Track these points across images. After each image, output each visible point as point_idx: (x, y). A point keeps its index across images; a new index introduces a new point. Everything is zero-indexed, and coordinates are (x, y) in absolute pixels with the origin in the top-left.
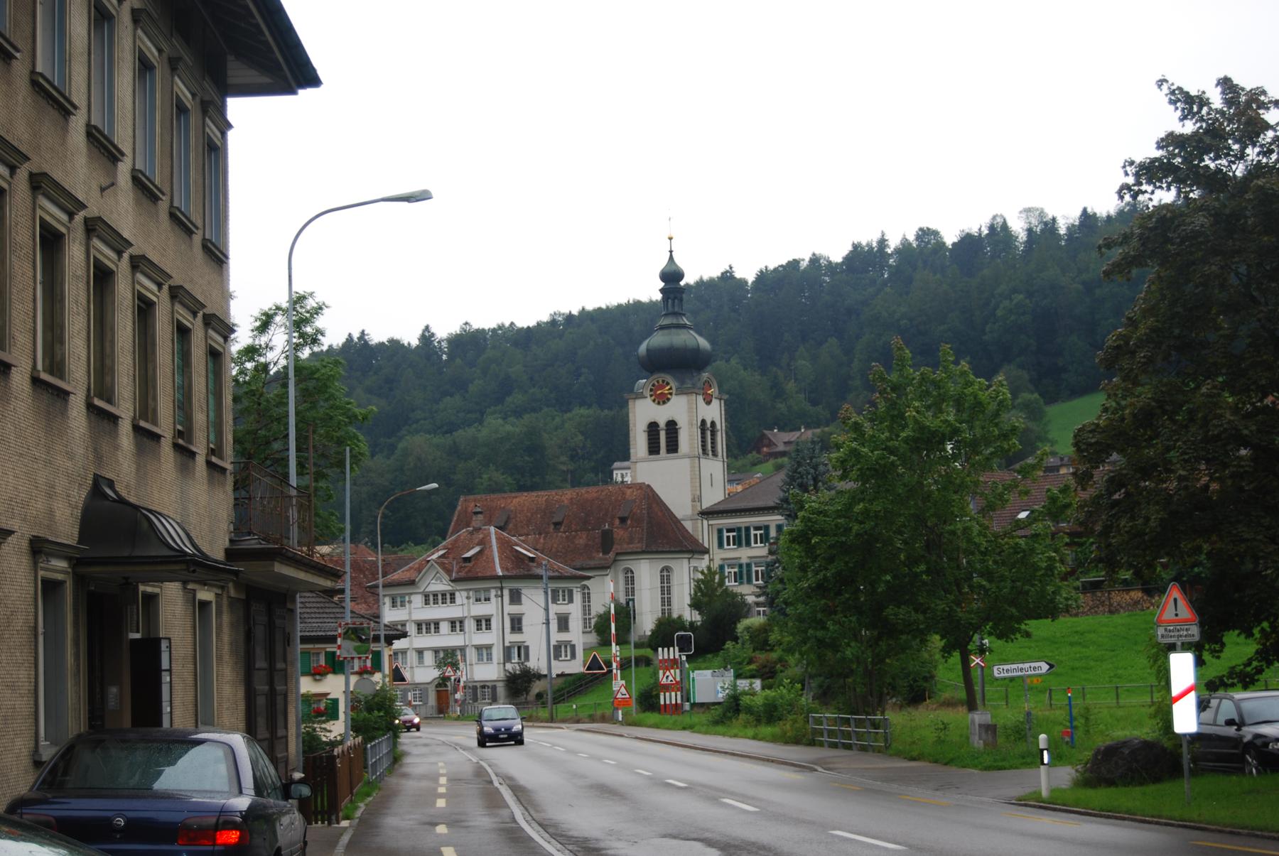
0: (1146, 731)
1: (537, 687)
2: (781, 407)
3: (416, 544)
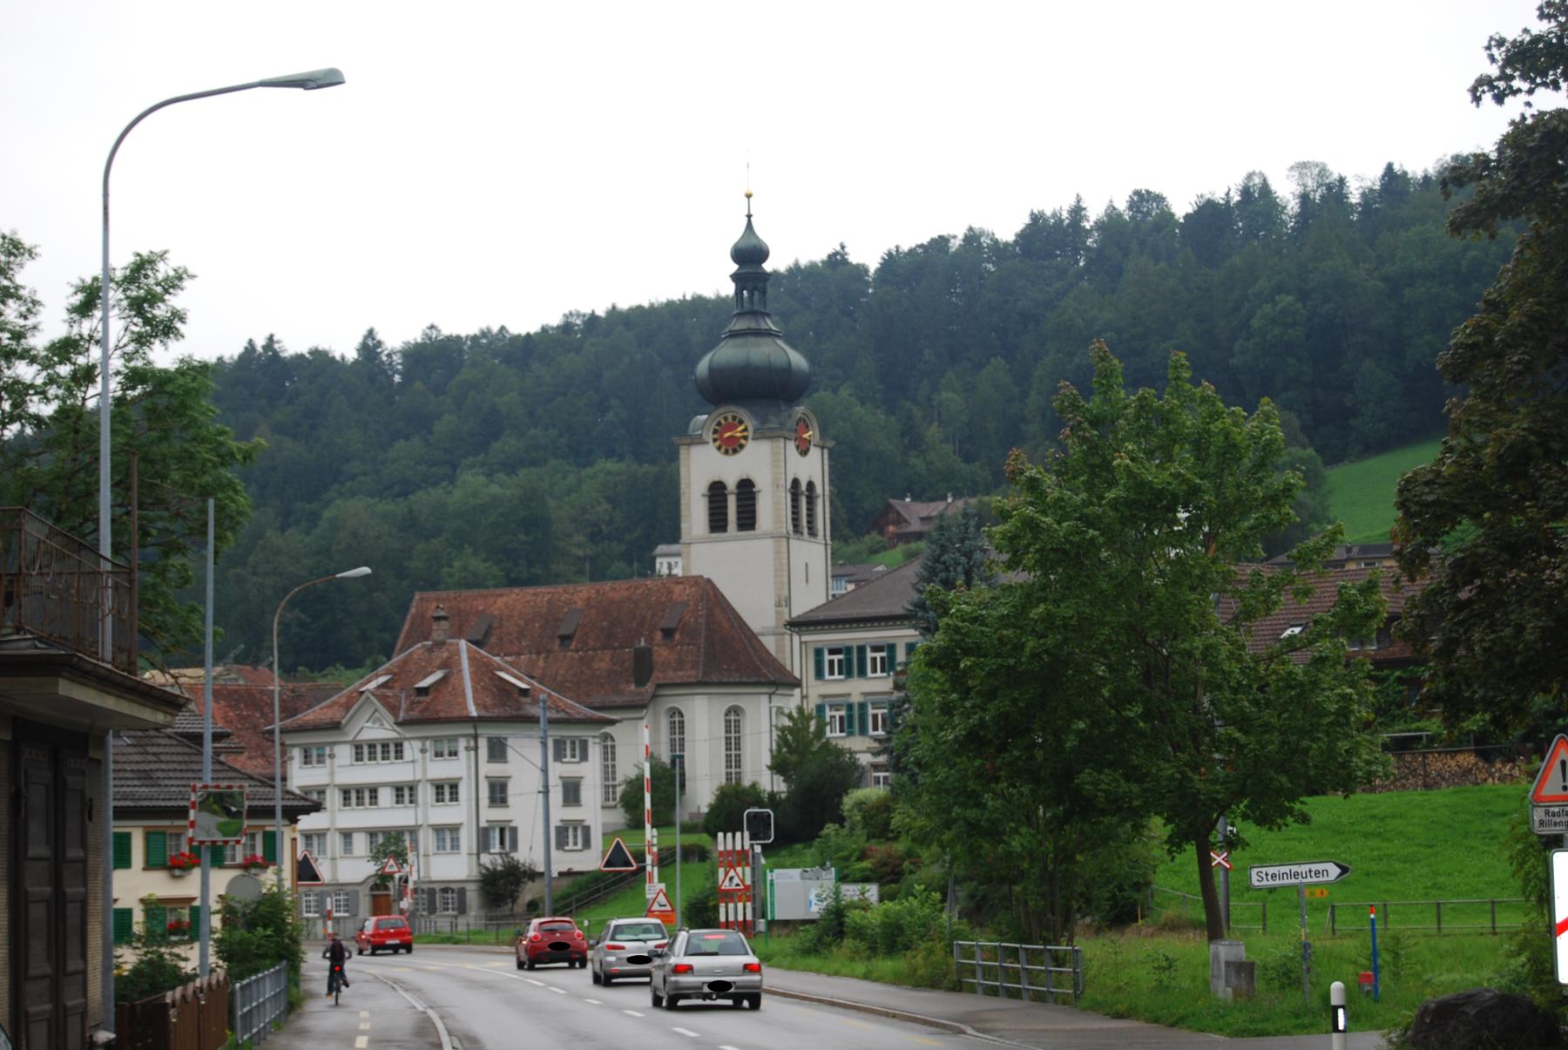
0: (1487, 973)
1: (529, 891)
2: (917, 462)
3: (347, 668)
